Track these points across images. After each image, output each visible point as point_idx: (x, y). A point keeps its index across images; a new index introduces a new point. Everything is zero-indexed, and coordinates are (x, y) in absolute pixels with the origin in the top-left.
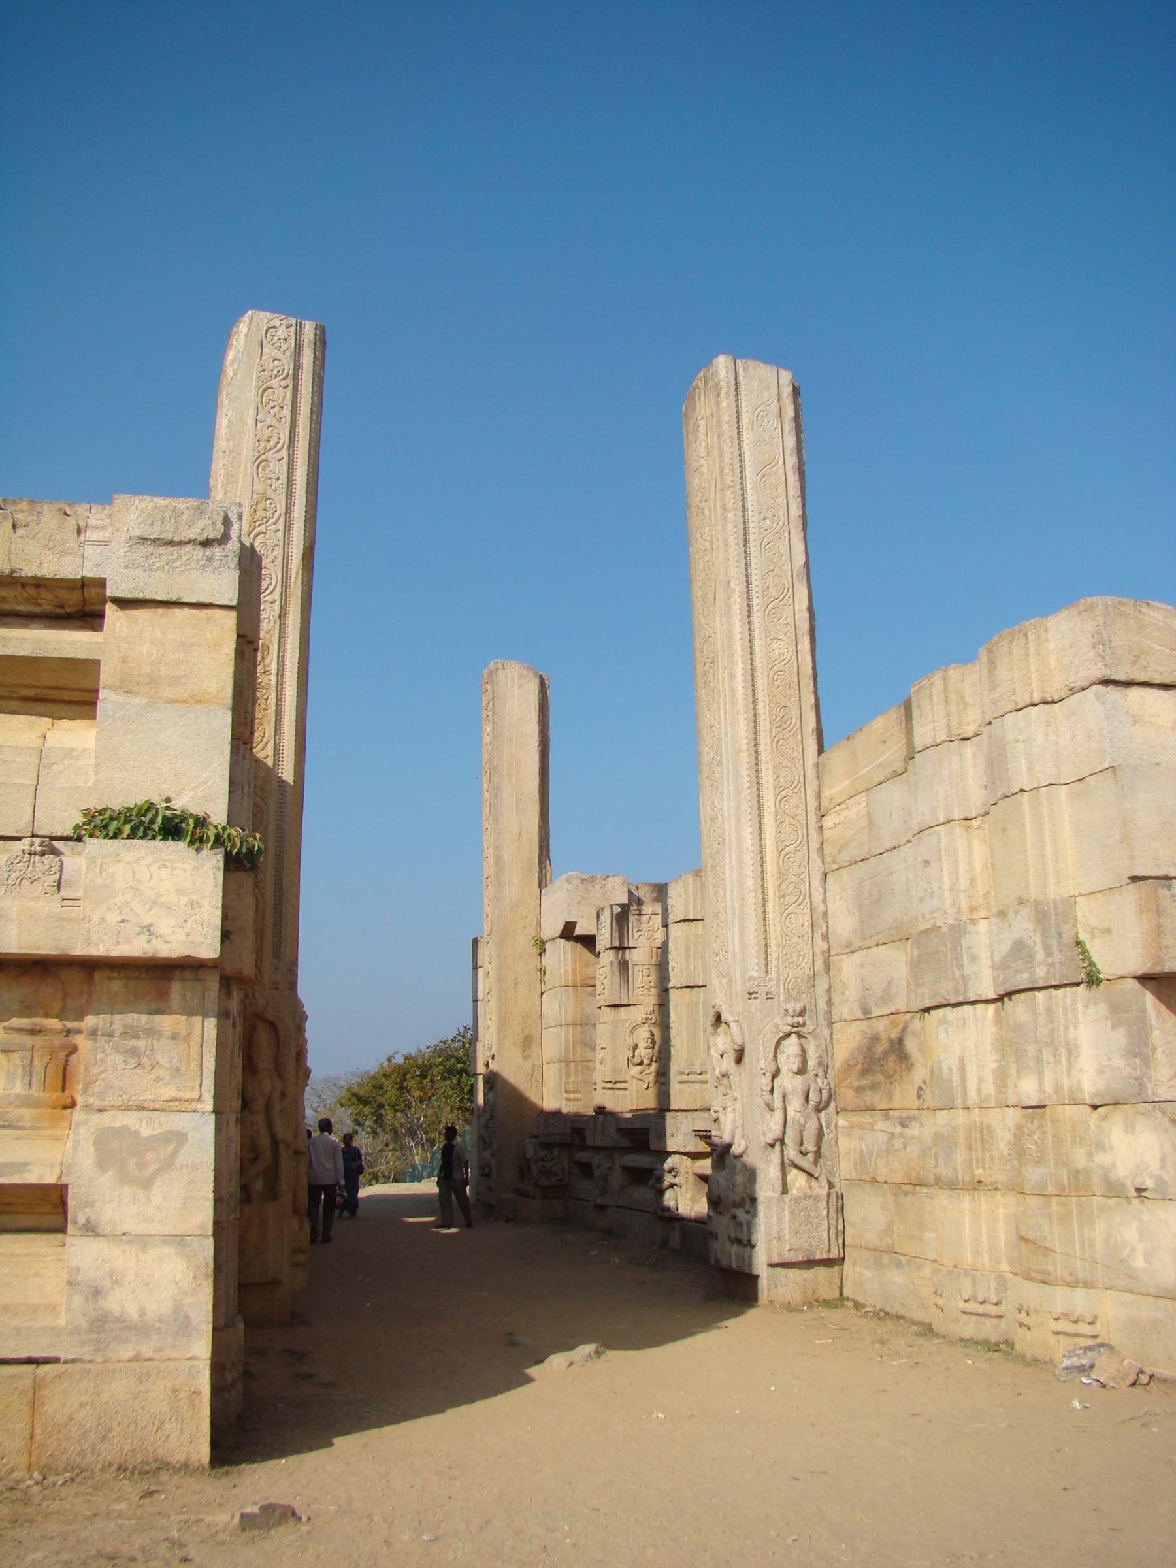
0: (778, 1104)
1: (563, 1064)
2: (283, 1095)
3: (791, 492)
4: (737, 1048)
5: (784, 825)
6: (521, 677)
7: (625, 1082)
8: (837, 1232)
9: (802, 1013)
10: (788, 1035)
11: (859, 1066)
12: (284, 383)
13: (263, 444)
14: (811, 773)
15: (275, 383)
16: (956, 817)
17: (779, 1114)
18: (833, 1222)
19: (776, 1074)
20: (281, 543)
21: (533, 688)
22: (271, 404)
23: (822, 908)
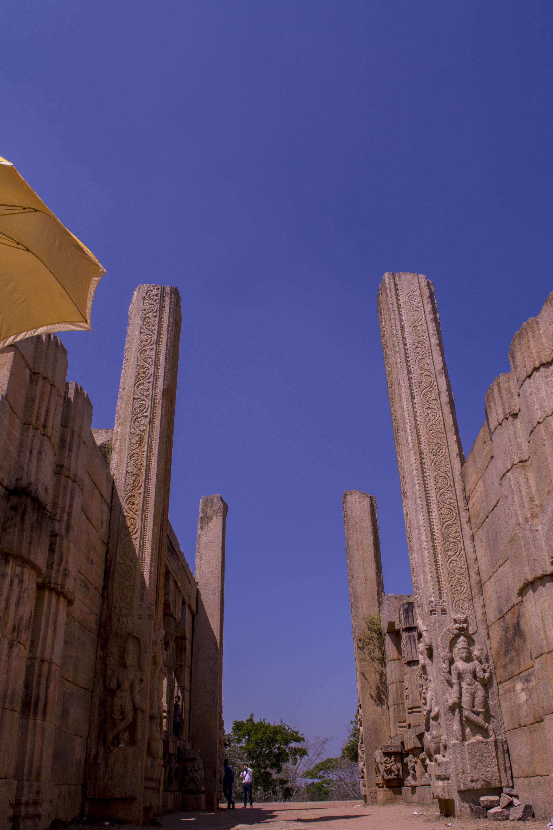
0: (454, 680)
1: (396, 706)
2: (141, 680)
3: (431, 333)
4: (427, 647)
5: (443, 509)
6: (359, 497)
7: (420, 707)
8: (505, 768)
9: (466, 621)
10: (457, 636)
11: (503, 650)
12: (154, 314)
13: (143, 343)
14: (457, 478)
15: (150, 315)
16: (516, 462)
17: (456, 687)
18: (501, 761)
19: (451, 662)
20: (151, 388)
21: (366, 502)
22: (148, 324)
23: (474, 557)
